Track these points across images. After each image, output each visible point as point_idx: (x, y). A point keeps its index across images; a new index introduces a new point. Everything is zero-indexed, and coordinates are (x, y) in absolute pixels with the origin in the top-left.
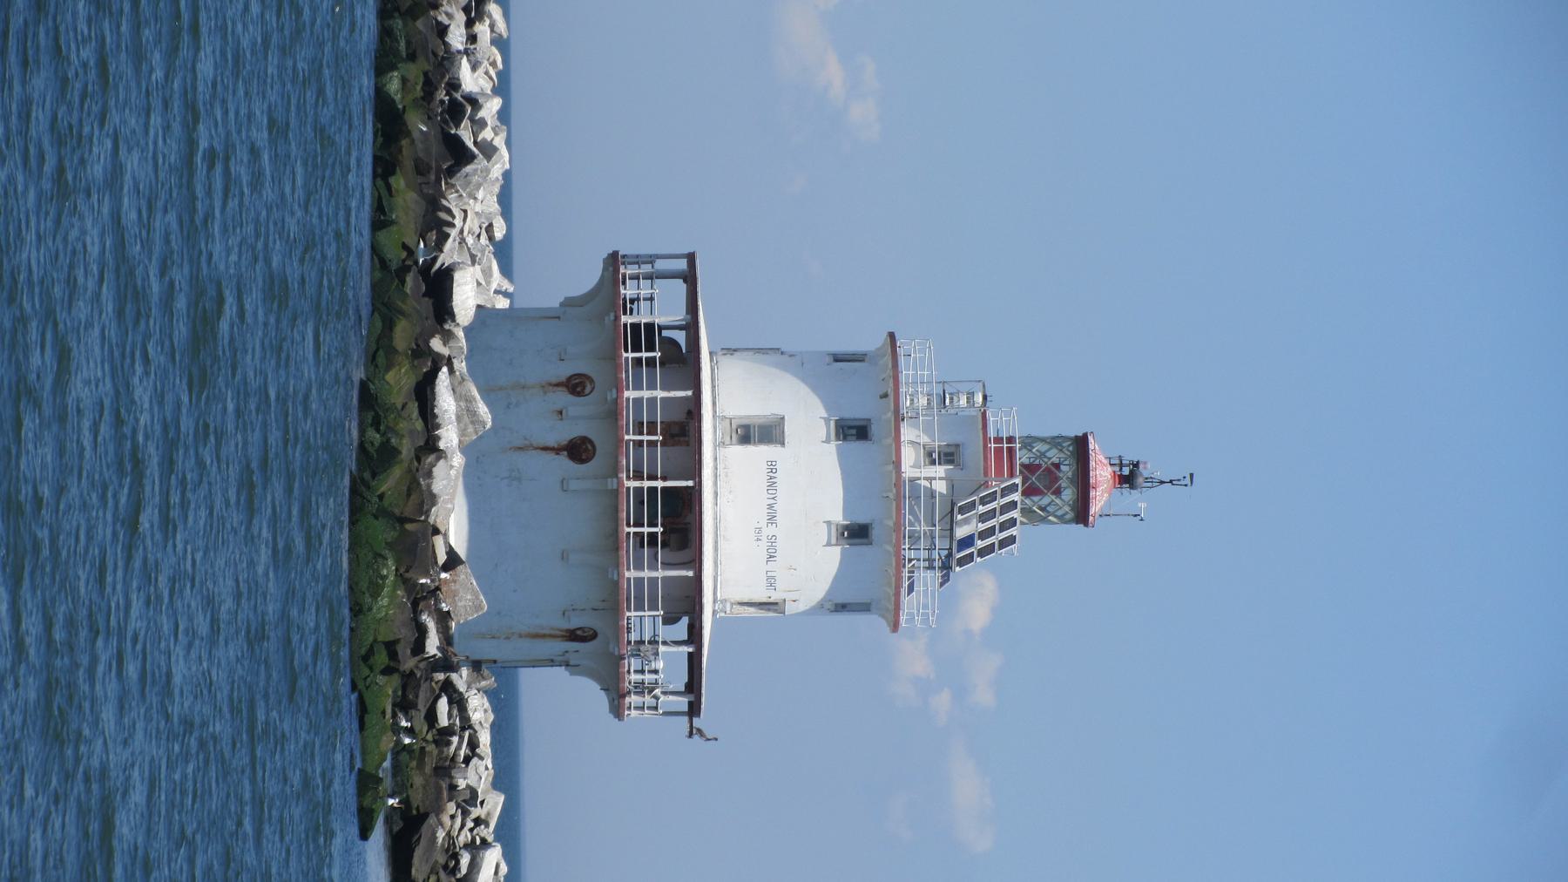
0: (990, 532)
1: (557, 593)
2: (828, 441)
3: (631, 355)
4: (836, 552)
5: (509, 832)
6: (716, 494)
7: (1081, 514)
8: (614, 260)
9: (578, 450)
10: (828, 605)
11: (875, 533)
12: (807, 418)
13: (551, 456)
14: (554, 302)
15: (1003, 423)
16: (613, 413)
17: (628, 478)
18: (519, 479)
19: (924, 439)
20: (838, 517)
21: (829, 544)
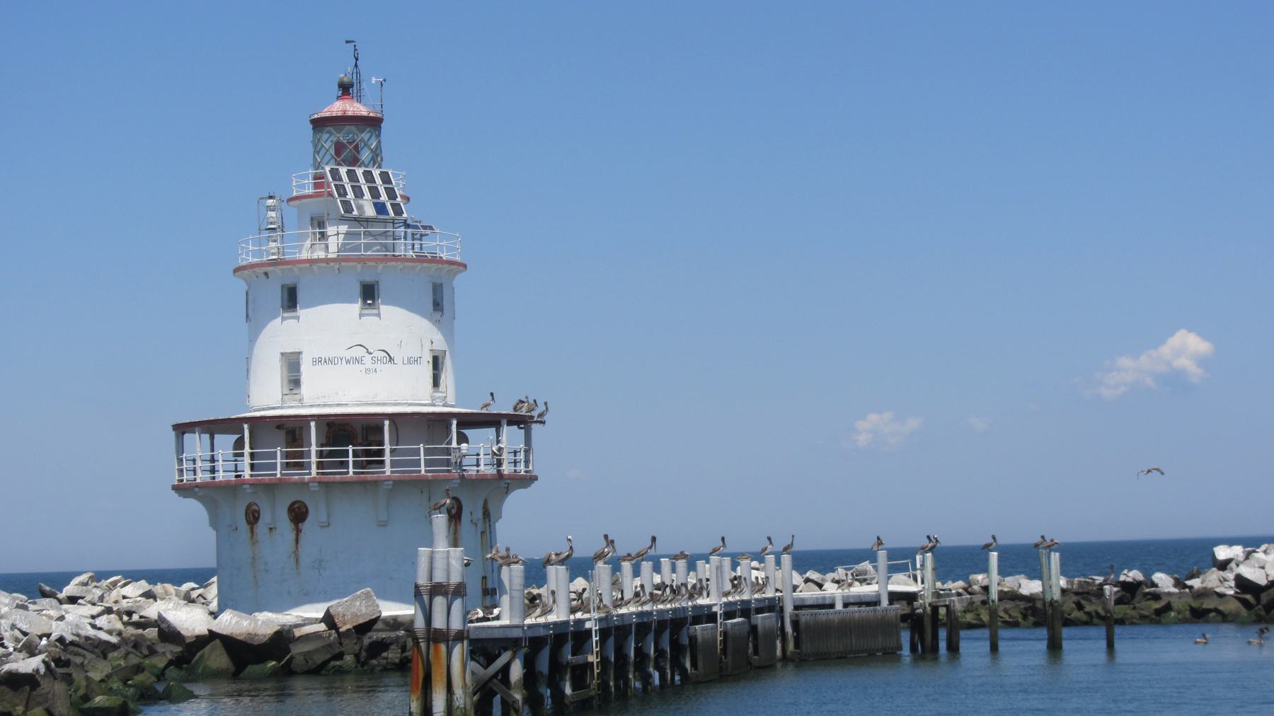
0: (374, 193)
2: (298, 318)
3: (351, 470)
4: (384, 309)
6: (338, 405)
7: (373, 123)
8: (182, 489)
9: (298, 514)
10: (438, 315)
11: (369, 279)
12: (281, 334)
13: (302, 535)
14: (212, 534)
17: (310, 474)
18: (321, 561)
19: (308, 243)
20: (356, 307)
21: (379, 315)
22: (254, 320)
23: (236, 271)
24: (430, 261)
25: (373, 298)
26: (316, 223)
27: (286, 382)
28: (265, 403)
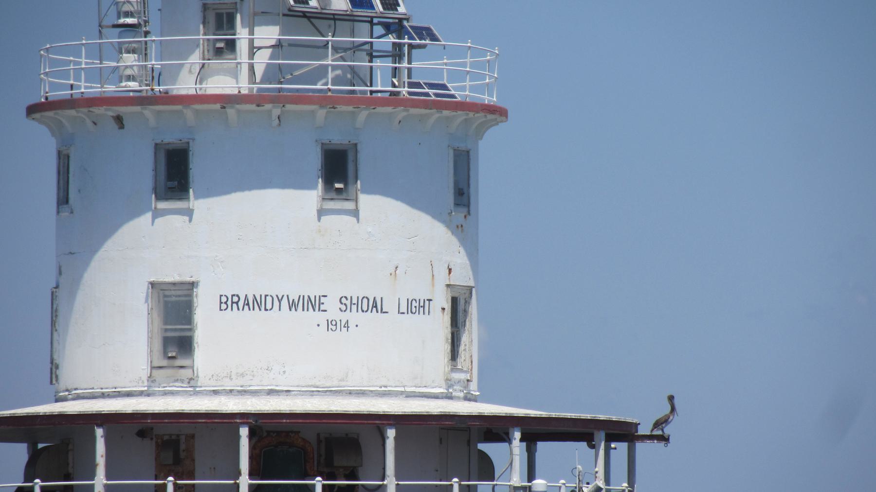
2: (189, 213)
6: (271, 392)
10: (459, 216)
11: (338, 138)
12: (152, 245)
19: (195, 59)
20: (311, 197)
21: (355, 213)
22: (79, 207)
23: (33, 110)
24: (438, 106)
25: (344, 179)
26: (212, 18)
27: (158, 345)
28: (108, 383)
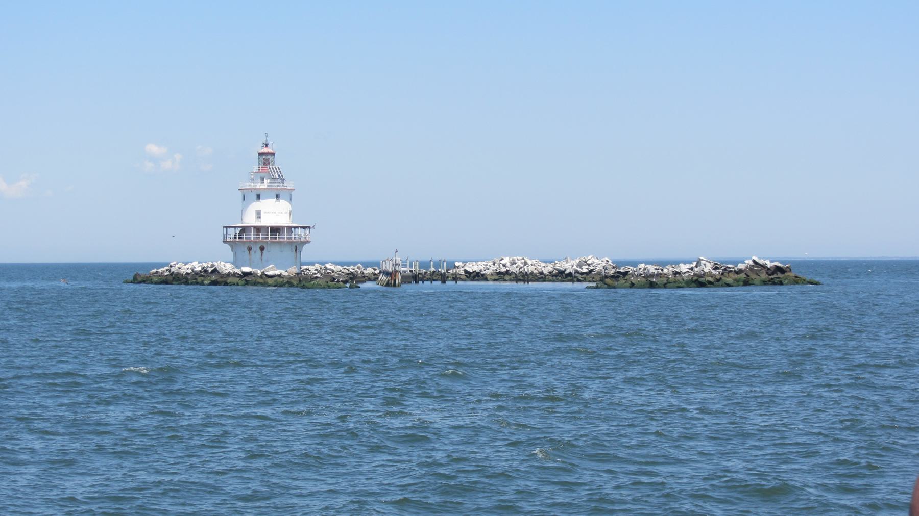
1: (288, 253)
5: (323, 263)
7: (273, 154)
8: (225, 242)
9: (262, 249)
12: (256, 206)
15: (255, 169)
16: (255, 242)
20: (275, 200)
